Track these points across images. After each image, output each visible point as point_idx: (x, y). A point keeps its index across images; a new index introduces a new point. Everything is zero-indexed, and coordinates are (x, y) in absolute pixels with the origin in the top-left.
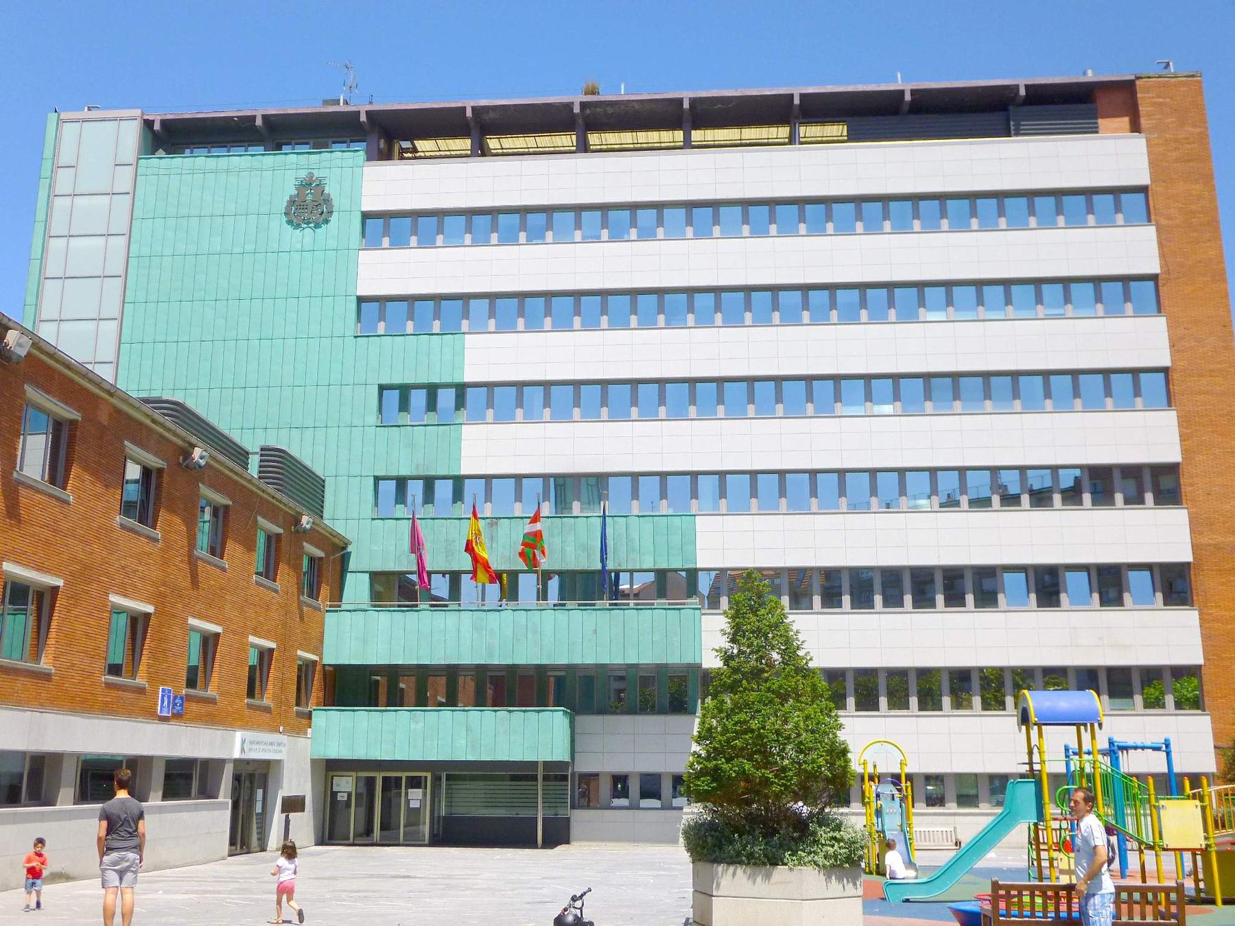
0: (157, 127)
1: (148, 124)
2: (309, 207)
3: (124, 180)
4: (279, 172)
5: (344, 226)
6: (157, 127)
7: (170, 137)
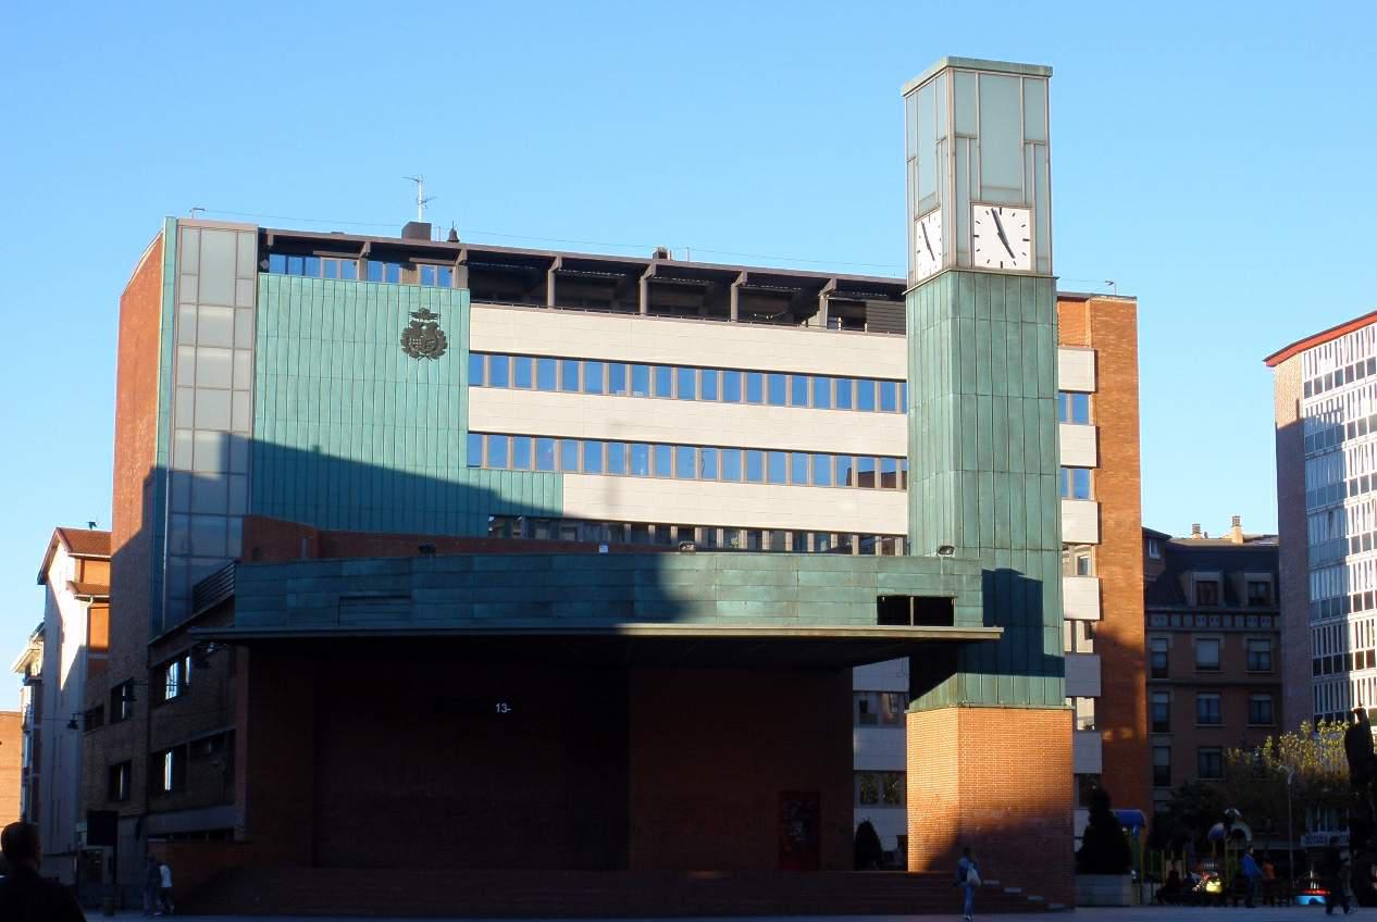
0: (270, 242)
1: (262, 235)
2: (425, 339)
3: (246, 289)
5: (452, 363)
6: (270, 242)
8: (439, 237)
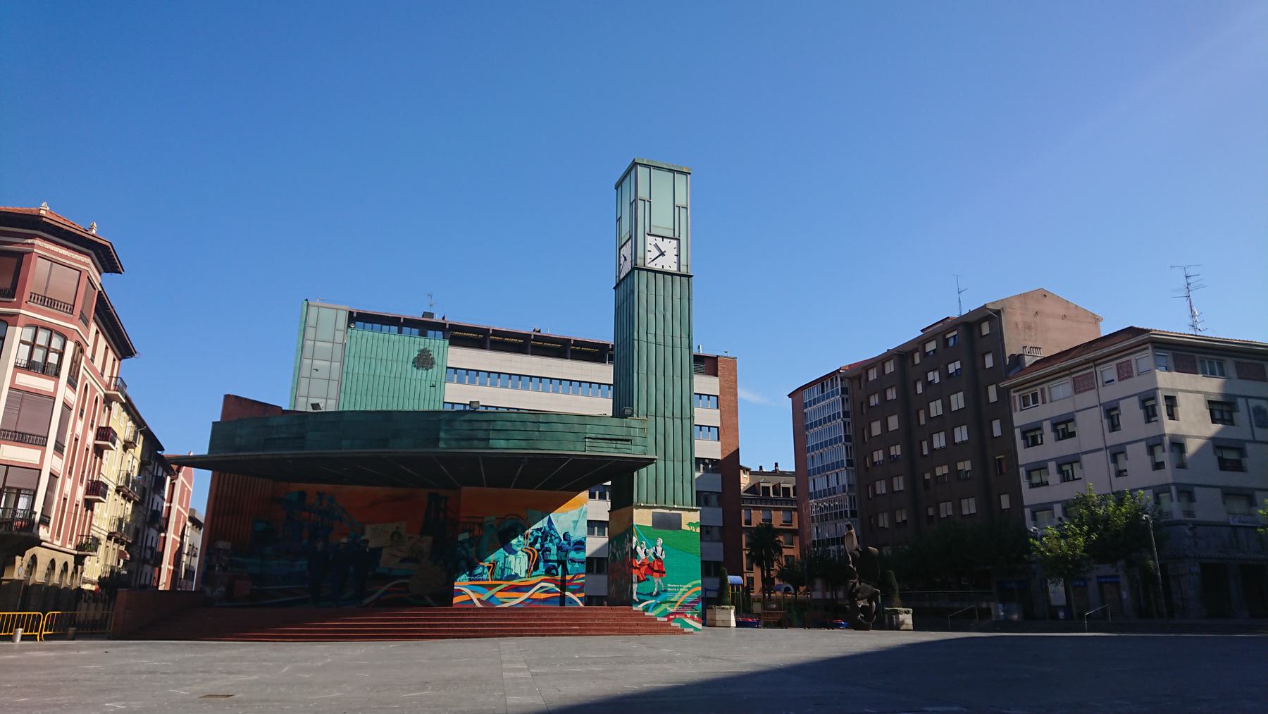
1: (351, 313)
2: (424, 360)
4: (413, 343)
7: (356, 318)
8: (437, 318)
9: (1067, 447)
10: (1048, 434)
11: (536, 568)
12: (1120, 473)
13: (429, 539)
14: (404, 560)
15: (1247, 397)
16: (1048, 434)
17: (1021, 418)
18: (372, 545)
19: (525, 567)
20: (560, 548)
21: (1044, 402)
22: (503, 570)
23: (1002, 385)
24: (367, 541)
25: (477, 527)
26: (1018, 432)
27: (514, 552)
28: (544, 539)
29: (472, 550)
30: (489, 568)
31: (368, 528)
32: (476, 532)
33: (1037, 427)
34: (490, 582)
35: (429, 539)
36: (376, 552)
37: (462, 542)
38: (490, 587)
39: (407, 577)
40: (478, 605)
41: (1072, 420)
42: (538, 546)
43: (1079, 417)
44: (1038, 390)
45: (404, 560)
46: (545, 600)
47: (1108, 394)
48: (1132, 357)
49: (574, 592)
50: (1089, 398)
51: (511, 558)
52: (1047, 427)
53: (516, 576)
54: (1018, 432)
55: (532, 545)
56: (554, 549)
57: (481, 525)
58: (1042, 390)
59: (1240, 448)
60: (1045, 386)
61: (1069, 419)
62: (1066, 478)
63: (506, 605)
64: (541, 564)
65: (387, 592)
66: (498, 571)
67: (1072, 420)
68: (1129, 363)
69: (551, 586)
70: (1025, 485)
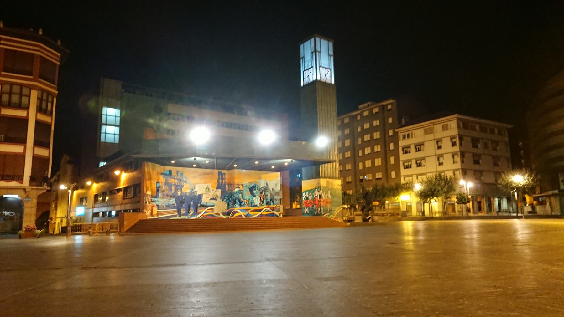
9: (419, 155)
10: (413, 149)
11: (263, 202)
12: (440, 164)
13: (220, 191)
14: (211, 199)
15: (482, 139)
16: (413, 149)
17: (402, 143)
18: (199, 193)
19: (259, 202)
20: (271, 195)
21: (412, 137)
22: (252, 203)
23: (396, 130)
24: (196, 191)
25: (241, 186)
26: (400, 149)
27: (255, 196)
28: (266, 190)
29: (240, 195)
30: (242, 202)
31: (197, 186)
32: (241, 188)
33: (409, 147)
34: (247, 208)
35: (220, 191)
36: (200, 197)
37: (236, 192)
38: (248, 210)
39: (213, 206)
40: (244, 217)
41: (423, 144)
42: (263, 193)
43: (426, 144)
44: (410, 133)
45: (211, 199)
46: (267, 215)
47: (438, 136)
48: (448, 123)
49: (277, 211)
50: (431, 136)
51: (254, 198)
52: (413, 147)
53: (256, 206)
54: (400, 149)
55: (261, 193)
56: (269, 195)
57: (242, 185)
58: (412, 133)
59: (479, 156)
60: (413, 131)
61: (422, 144)
62: (419, 165)
63: (254, 217)
64: (265, 201)
65: (206, 212)
66: (250, 204)
67: (423, 144)
68: (447, 125)
69: (268, 209)
70: (402, 168)
